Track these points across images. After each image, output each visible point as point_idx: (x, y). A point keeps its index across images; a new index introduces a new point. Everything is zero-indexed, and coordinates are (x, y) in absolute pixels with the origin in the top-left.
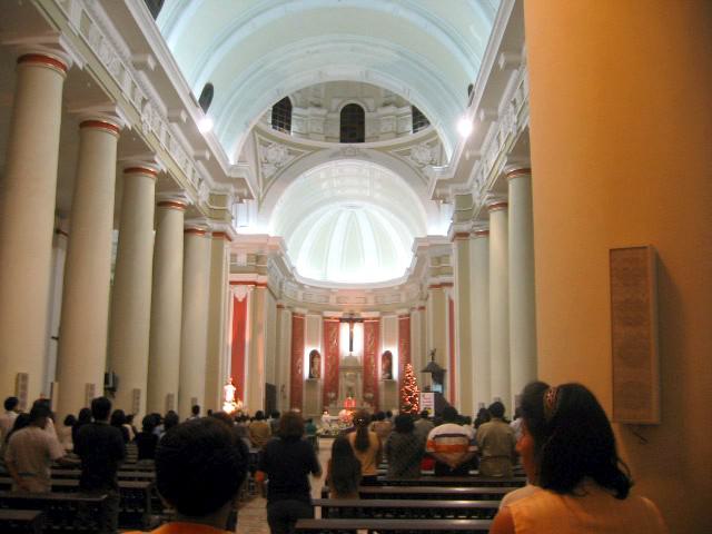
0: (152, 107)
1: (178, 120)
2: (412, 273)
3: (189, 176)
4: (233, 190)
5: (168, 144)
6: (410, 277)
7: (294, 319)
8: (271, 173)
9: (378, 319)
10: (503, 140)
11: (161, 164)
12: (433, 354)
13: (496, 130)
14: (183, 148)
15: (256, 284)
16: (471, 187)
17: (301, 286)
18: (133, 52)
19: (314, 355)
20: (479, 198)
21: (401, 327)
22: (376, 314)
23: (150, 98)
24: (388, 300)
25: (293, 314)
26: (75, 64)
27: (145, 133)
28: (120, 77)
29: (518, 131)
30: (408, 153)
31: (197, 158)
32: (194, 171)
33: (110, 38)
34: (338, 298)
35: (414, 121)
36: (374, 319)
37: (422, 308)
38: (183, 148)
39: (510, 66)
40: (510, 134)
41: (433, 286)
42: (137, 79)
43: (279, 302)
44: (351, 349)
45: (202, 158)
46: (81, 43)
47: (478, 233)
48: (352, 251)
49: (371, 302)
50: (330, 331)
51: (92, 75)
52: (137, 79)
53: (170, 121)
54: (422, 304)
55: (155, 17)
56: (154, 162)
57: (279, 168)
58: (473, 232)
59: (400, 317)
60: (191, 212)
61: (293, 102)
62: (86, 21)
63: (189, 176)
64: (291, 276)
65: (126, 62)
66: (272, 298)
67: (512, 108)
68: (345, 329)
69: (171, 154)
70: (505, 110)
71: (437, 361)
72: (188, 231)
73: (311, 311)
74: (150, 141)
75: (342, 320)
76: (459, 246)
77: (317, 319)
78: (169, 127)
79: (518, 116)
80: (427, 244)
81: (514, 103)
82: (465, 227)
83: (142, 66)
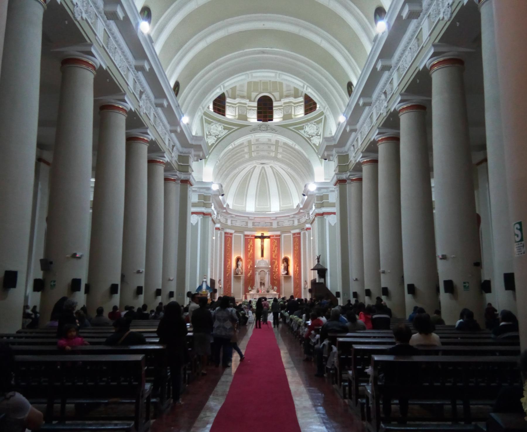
4: (193, 152)
5: (155, 122)
7: (225, 237)
8: (213, 142)
9: (280, 236)
10: (375, 118)
11: (151, 136)
13: (417, 27)
14: (123, 52)
16: (349, 149)
18: (156, 97)
19: (238, 259)
20: (354, 157)
22: (278, 233)
24: (287, 224)
26: (101, 66)
27: (142, 114)
28: (95, 24)
29: (387, 112)
30: (302, 128)
31: (171, 131)
32: (169, 140)
33: (121, 49)
35: (306, 107)
36: (277, 236)
38: (123, 52)
41: (318, 215)
42: (156, 113)
43: (218, 225)
44: (262, 255)
45: (175, 132)
47: (352, 180)
49: (275, 225)
50: (249, 241)
51: (158, 143)
52: (137, 77)
56: (147, 134)
58: (349, 179)
59: (294, 234)
60: (168, 167)
61: (226, 95)
62: (107, 37)
65: (130, 65)
67: (383, 96)
70: (379, 97)
72: (166, 179)
73: (236, 232)
74: (144, 119)
76: (340, 187)
78: (155, 111)
82: (344, 176)
83: (161, 106)
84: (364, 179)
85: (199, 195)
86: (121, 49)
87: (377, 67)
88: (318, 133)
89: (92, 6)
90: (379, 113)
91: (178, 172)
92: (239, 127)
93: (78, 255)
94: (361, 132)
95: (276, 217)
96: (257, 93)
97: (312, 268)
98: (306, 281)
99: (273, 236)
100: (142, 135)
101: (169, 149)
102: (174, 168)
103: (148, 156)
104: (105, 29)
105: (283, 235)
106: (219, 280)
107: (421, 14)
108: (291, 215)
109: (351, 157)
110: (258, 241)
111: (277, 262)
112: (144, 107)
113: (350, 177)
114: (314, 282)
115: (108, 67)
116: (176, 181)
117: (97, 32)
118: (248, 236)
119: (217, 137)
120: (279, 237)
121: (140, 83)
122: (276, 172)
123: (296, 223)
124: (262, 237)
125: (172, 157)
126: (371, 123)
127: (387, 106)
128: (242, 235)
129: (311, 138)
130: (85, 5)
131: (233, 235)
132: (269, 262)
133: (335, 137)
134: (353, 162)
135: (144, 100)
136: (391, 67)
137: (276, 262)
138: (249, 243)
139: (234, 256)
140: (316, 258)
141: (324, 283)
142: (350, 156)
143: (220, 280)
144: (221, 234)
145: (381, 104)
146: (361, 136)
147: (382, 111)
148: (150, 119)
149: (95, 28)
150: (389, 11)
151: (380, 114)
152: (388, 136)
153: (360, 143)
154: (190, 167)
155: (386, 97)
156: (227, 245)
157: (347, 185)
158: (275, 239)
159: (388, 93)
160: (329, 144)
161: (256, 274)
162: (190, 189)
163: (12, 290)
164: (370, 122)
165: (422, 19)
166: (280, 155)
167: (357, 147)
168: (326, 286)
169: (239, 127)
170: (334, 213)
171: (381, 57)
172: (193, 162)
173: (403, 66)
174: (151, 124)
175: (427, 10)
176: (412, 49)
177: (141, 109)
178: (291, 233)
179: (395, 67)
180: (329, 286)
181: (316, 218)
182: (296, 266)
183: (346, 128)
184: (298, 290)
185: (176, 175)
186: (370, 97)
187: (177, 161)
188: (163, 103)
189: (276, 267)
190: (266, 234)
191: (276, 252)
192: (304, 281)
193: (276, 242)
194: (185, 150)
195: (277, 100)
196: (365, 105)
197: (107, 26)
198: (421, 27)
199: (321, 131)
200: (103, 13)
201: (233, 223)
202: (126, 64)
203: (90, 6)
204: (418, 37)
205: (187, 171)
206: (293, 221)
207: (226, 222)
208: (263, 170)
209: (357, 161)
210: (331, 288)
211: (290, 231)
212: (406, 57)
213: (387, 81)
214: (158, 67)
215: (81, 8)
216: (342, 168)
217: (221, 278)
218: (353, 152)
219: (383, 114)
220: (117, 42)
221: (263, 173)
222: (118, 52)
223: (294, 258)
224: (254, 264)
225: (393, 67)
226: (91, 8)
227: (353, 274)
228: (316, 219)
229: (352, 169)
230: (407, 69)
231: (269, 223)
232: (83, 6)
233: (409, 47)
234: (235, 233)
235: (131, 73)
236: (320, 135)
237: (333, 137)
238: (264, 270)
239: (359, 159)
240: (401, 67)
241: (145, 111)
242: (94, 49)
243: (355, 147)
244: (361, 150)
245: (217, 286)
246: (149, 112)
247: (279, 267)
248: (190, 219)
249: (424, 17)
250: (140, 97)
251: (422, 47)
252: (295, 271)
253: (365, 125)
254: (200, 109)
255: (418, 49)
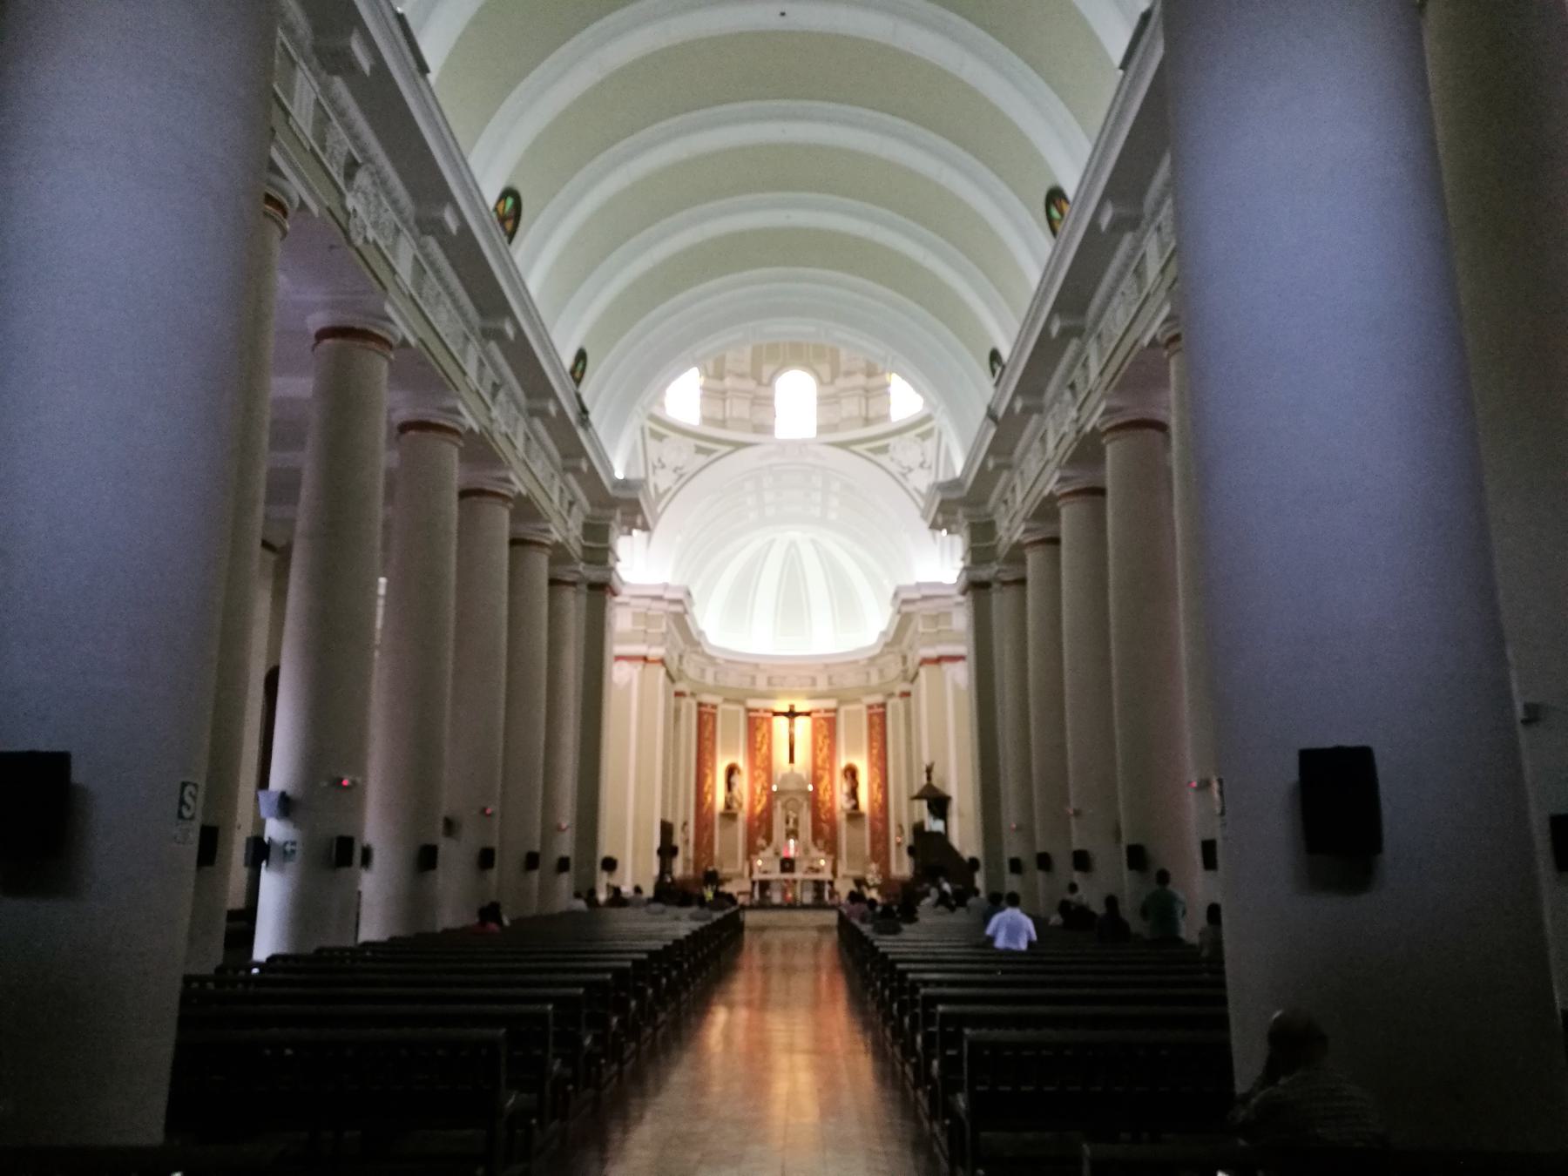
2: (889, 639)
3: (555, 497)
5: (527, 452)
6: (887, 645)
7: (700, 715)
9: (835, 711)
10: (1051, 444)
12: (929, 771)
15: (645, 659)
16: (995, 509)
17: (711, 659)
18: (529, 396)
19: (731, 771)
20: (1008, 529)
21: (871, 726)
22: (831, 704)
23: (369, 160)
25: (700, 705)
27: (497, 436)
28: (393, 248)
29: (1078, 432)
37: (906, 694)
38: (455, 301)
40: (1064, 435)
43: (680, 686)
44: (792, 760)
47: (1005, 583)
48: (793, 603)
49: (822, 685)
50: (755, 725)
52: (567, 485)
53: (423, 233)
54: (905, 687)
57: (681, 476)
58: (996, 579)
59: (870, 707)
60: (560, 554)
63: (555, 497)
64: (698, 644)
67: (1068, 395)
68: (780, 724)
69: (530, 464)
71: (935, 782)
72: (553, 582)
73: (726, 700)
77: (738, 712)
79: (1080, 409)
80: (917, 595)
81: (1072, 387)
82: (984, 574)
83: (543, 414)
84: (1029, 582)
85: (635, 615)
86: (451, 294)
93: (488, 811)
100: (541, 534)
101: (481, 391)
102: (574, 555)
105: (843, 710)
110: (780, 724)
112: (502, 421)
116: (578, 586)
123: (875, 680)
124: (792, 714)
128: (741, 709)
132: (807, 776)
134: (1005, 539)
136: (1084, 330)
143: (685, 824)
147: (1066, 428)
148: (464, 373)
150: (1076, 198)
153: (1019, 497)
155: (1075, 395)
157: (994, 595)
158: (824, 719)
162: (613, 602)
163: (432, 873)
164: (1135, 286)
165: (1145, 233)
167: (1086, 387)
171: (1057, 308)
174: (469, 387)
175: (1155, 213)
177: (496, 425)
184: (880, 847)
185: (577, 572)
186: (1011, 453)
187: (581, 538)
188: (443, 218)
189: (826, 790)
191: (825, 750)
193: (828, 727)
194: (598, 512)
197: (421, 247)
199: (930, 457)
202: (462, 327)
206: (868, 674)
213: (1126, 266)
216: (979, 553)
220: (441, 279)
223: (872, 765)
225: (1087, 330)
228: (923, 672)
232: (368, 213)
236: (930, 467)
239: (1017, 536)
241: (504, 428)
242: (277, 149)
244: (1021, 515)
245: (678, 839)
251: (1148, 296)
253: (1030, 456)
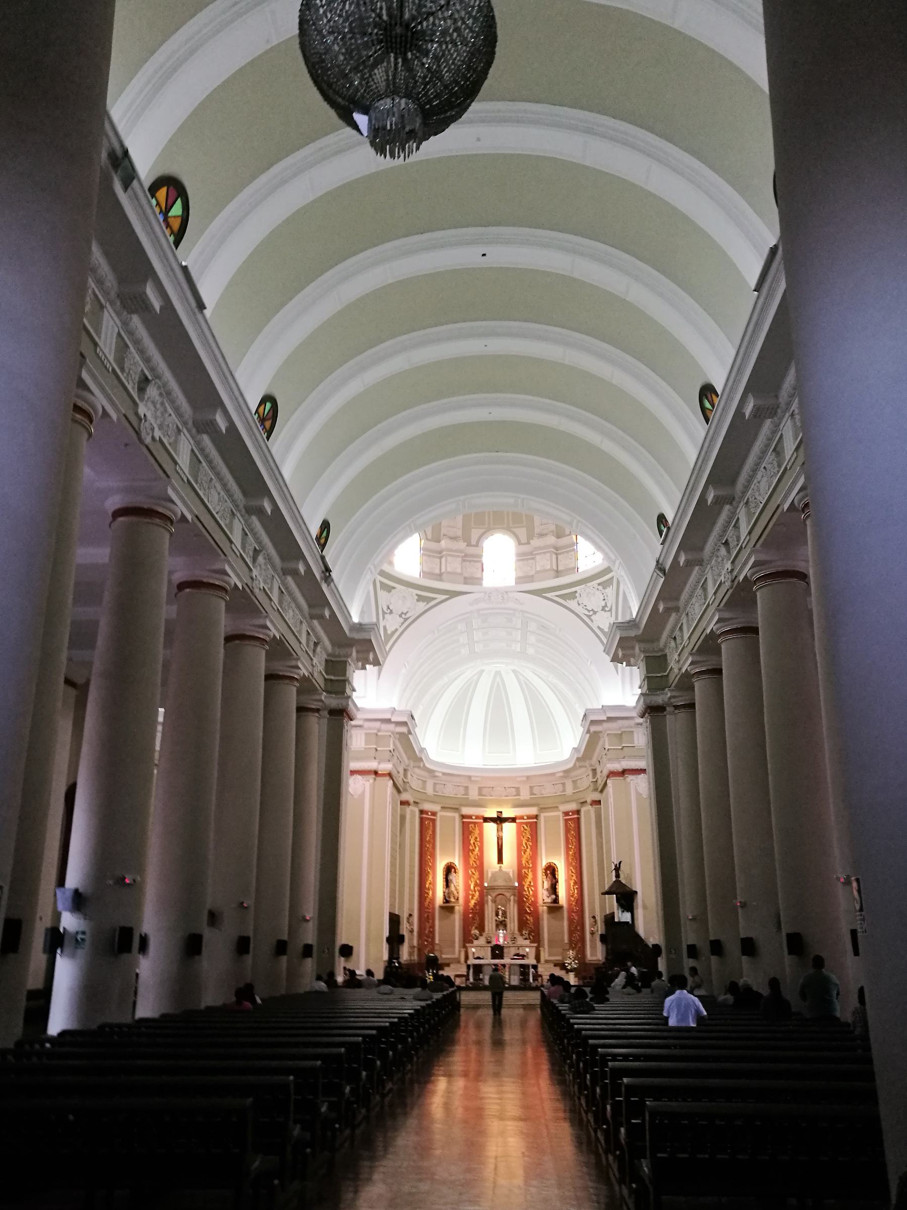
0: (265, 558)
1: (321, 617)
3: (303, 640)
5: (281, 602)
7: (422, 820)
9: (536, 817)
10: (711, 590)
12: (617, 869)
13: (774, 432)
17: (431, 772)
18: (283, 558)
22: (533, 811)
23: (158, 377)
24: (549, 790)
25: (422, 812)
26: (274, 636)
27: (256, 591)
28: (175, 444)
29: (733, 581)
34: (480, 789)
36: (529, 817)
38: (225, 486)
39: (668, 611)
46: (189, 489)
49: (525, 795)
54: (596, 796)
55: (177, 248)
57: (406, 620)
58: (670, 705)
59: (566, 814)
60: (306, 686)
63: (303, 640)
64: (421, 760)
65: (237, 506)
66: (395, 792)
67: (723, 551)
72: (301, 710)
75: (486, 820)
79: (733, 562)
81: (726, 544)
82: (660, 699)
87: (679, 560)
88: (606, 606)
89: (173, 414)
90: (717, 580)
91: (324, 693)
92: (448, 596)
94: (747, 503)
95: (528, 777)
96: (483, 530)
97: (607, 888)
98: (594, 917)
99: (522, 818)
103: (266, 667)
104: (192, 451)
105: (542, 816)
106: (408, 915)
107: (779, 411)
108: (558, 772)
109: (671, 661)
111: (533, 874)
113: (673, 700)
114: (609, 920)
115: (197, 517)
117: (178, 456)
118: (470, 817)
119: (403, 616)
120: (535, 820)
121: (254, 535)
122: (526, 683)
124: (499, 820)
125: (313, 666)
126: (705, 599)
127: (732, 570)
128: (457, 815)
129: (591, 615)
130: (159, 413)
131: (438, 815)
133: (637, 620)
135: (260, 566)
137: (530, 876)
138: (471, 833)
139: (440, 862)
140: (613, 867)
141: (630, 923)
142: (668, 658)
143: (410, 915)
144: (413, 813)
145: (721, 565)
146: (688, 620)
149: (175, 451)
151: (721, 583)
152: (713, 667)
153: (686, 636)
154: (350, 683)
156: (426, 837)
158: (526, 824)
159: (731, 545)
160: (626, 634)
161: (487, 901)
162: (348, 725)
165: (781, 419)
166: (389, 1123)
168: (636, 929)
169: (448, 596)
170: (643, 771)
172: (354, 672)
173: (755, 499)
176: (768, 470)
178: (559, 811)
179: (742, 497)
180: (641, 930)
181: (608, 781)
182: (572, 884)
183: (657, 606)
184: (577, 935)
190: (508, 813)
192: (589, 917)
195: (522, 542)
196: (720, 502)
198: (736, 517)
199: (611, 601)
200: (190, 423)
201: (437, 789)
203: (167, 415)
204: (777, 449)
205: (344, 692)
206: (564, 784)
207: (424, 787)
208: (498, 679)
209: (683, 670)
210: (645, 933)
211: (557, 807)
212: (759, 482)
214: (290, 510)
215: (152, 421)
217: (413, 910)
218: (674, 652)
219: (724, 583)
221: (498, 683)
222: (215, 487)
223: (568, 864)
224: (481, 878)
225: (737, 499)
226: (170, 418)
227: (687, 909)
229: (674, 685)
230: (761, 505)
231: (513, 790)
232: (156, 418)
233: (763, 466)
234: (440, 811)
235: (238, 518)
236: (610, 610)
237: (634, 621)
238: (504, 894)
240: (750, 499)
243: (678, 641)
245: (404, 929)
246: (269, 586)
247: (535, 886)
248: (348, 785)
249: (784, 416)
250: (254, 560)
252: (569, 896)
254: (370, 569)
255: (778, 472)
